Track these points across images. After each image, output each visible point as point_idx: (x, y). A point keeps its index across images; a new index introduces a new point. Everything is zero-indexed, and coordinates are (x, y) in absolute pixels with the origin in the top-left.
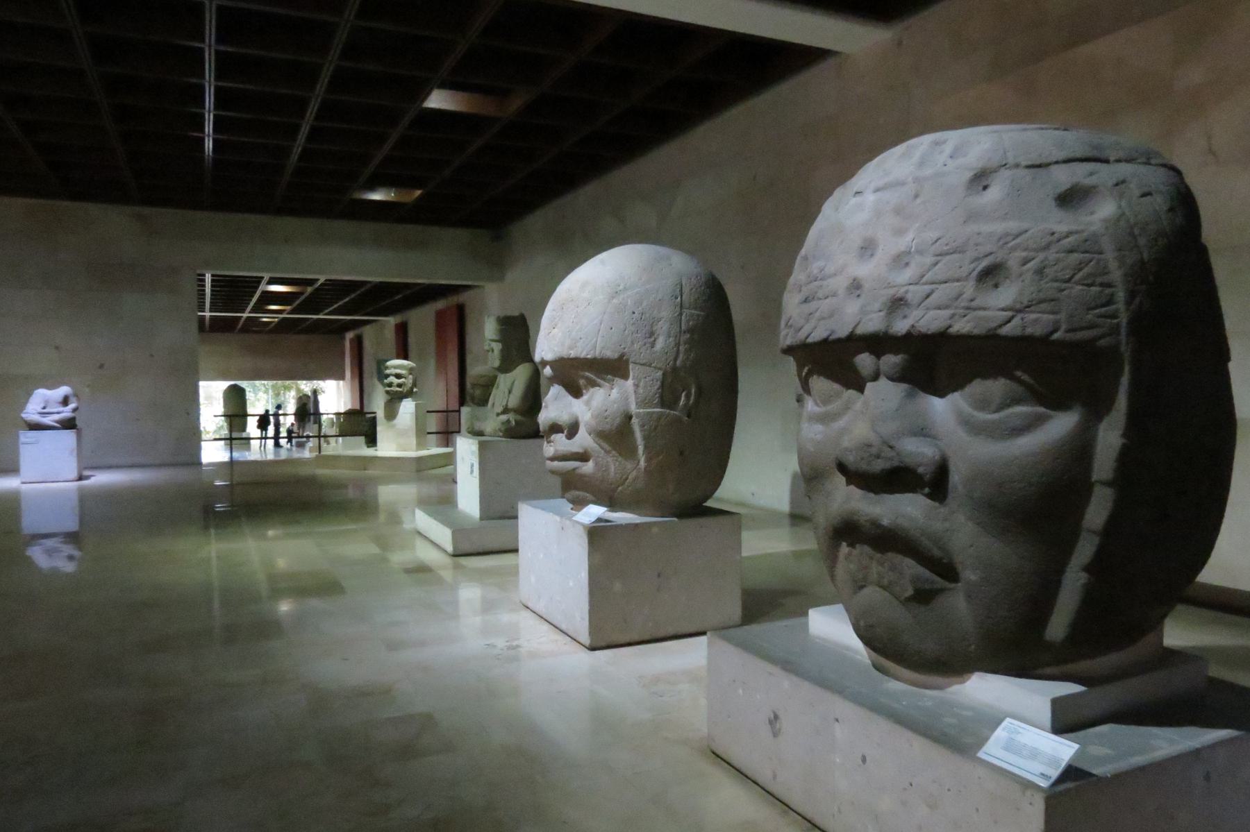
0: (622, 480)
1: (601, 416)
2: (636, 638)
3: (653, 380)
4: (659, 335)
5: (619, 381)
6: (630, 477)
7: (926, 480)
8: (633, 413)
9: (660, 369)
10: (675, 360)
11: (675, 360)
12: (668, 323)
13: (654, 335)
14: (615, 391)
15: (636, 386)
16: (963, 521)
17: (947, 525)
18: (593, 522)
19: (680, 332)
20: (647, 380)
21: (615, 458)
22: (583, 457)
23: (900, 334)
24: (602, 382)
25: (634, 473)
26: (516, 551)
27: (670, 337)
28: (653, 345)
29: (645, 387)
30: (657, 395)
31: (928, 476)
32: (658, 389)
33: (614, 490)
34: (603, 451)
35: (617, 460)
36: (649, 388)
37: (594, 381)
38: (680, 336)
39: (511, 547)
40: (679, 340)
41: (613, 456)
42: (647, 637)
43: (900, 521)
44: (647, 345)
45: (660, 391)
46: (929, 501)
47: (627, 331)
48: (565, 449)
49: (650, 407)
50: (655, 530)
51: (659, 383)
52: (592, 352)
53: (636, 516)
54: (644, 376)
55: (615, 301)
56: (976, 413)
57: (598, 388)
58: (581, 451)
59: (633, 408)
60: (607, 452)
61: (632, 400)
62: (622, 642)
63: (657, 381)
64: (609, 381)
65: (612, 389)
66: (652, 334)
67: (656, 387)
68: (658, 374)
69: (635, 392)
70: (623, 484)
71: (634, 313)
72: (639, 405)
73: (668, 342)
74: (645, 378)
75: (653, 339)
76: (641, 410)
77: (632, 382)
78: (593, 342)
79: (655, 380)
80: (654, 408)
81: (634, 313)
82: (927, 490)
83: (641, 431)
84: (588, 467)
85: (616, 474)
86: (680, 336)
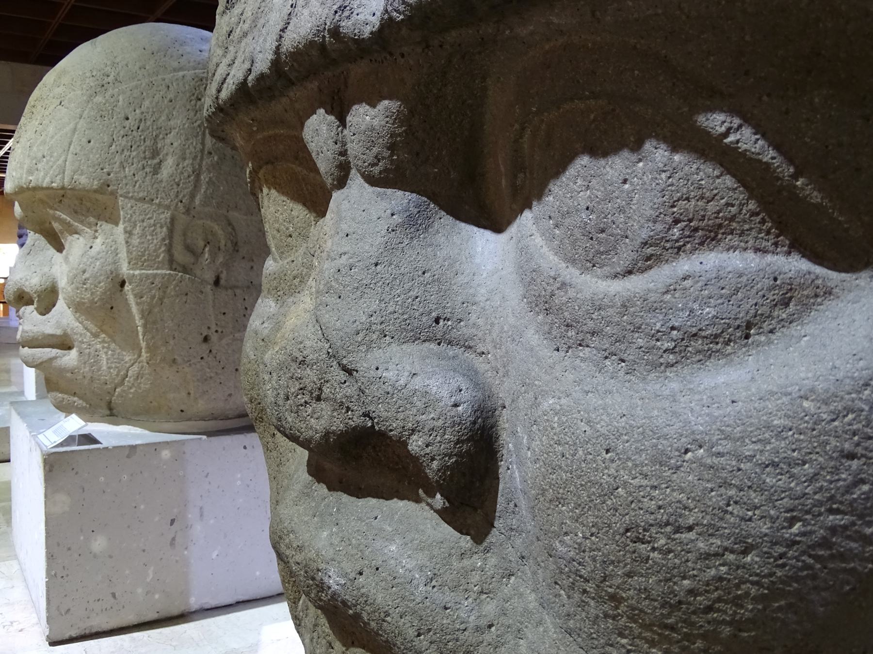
0: (119, 378)
1: (79, 278)
2: (131, 618)
3: (154, 225)
4: (167, 154)
5: (106, 227)
6: (130, 373)
7: (431, 475)
8: (125, 277)
9: (168, 207)
10: (192, 196)
11: (192, 196)
12: (183, 138)
13: (158, 154)
14: (99, 241)
15: (129, 233)
16: (533, 606)
17: (490, 608)
18: (61, 445)
19: (202, 151)
20: (145, 224)
21: (106, 345)
22: (64, 343)
23: (551, 181)
24: (80, 226)
25: (135, 368)
26: (9, 461)
27: (184, 159)
28: (156, 170)
29: (143, 235)
30: (163, 249)
31: (435, 465)
32: (164, 239)
33: (111, 393)
34: (89, 334)
35: (108, 348)
36: (149, 237)
37: (69, 225)
38: (202, 159)
39: (6, 458)
40: (200, 165)
41: (103, 341)
42: (152, 616)
43: (368, 584)
44: (148, 170)
45: (167, 242)
46: (447, 530)
47: (114, 147)
48: (35, 329)
49: (150, 267)
50: (166, 454)
51: (165, 229)
52: (58, 178)
53: (147, 432)
54: (141, 218)
55: (99, 99)
56: (571, 273)
57: (76, 236)
58: (59, 332)
59: (125, 269)
60: (95, 336)
61: (123, 255)
62: (106, 627)
63: (161, 227)
64: (90, 226)
65: (95, 238)
66: (155, 153)
67: (160, 237)
68: (162, 216)
69: (127, 242)
70: (122, 383)
71: (127, 119)
72: (133, 262)
73: (181, 166)
74: (143, 221)
75: (156, 161)
76: (137, 272)
77: (123, 226)
78: (60, 162)
79: (158, 225)
80: (157, 269)
81: (127, 119)
82: (439, 500)
83: (137, 304)
84: (71, 358)
85: (109, 368)
86: (202, 159)
